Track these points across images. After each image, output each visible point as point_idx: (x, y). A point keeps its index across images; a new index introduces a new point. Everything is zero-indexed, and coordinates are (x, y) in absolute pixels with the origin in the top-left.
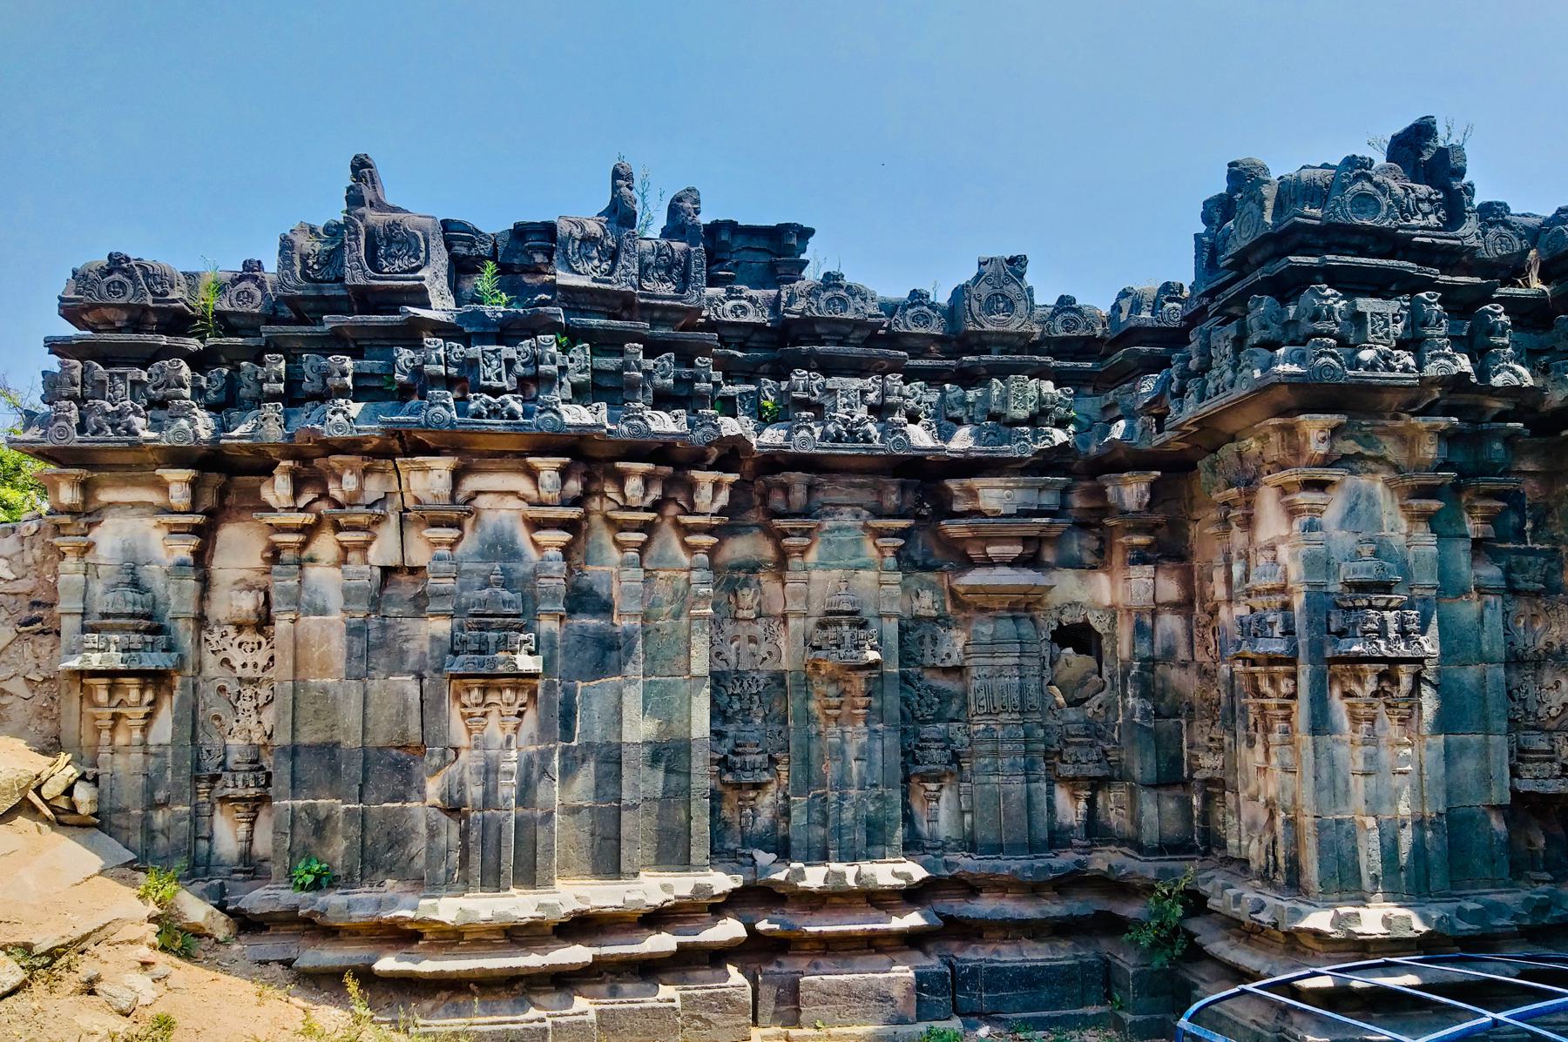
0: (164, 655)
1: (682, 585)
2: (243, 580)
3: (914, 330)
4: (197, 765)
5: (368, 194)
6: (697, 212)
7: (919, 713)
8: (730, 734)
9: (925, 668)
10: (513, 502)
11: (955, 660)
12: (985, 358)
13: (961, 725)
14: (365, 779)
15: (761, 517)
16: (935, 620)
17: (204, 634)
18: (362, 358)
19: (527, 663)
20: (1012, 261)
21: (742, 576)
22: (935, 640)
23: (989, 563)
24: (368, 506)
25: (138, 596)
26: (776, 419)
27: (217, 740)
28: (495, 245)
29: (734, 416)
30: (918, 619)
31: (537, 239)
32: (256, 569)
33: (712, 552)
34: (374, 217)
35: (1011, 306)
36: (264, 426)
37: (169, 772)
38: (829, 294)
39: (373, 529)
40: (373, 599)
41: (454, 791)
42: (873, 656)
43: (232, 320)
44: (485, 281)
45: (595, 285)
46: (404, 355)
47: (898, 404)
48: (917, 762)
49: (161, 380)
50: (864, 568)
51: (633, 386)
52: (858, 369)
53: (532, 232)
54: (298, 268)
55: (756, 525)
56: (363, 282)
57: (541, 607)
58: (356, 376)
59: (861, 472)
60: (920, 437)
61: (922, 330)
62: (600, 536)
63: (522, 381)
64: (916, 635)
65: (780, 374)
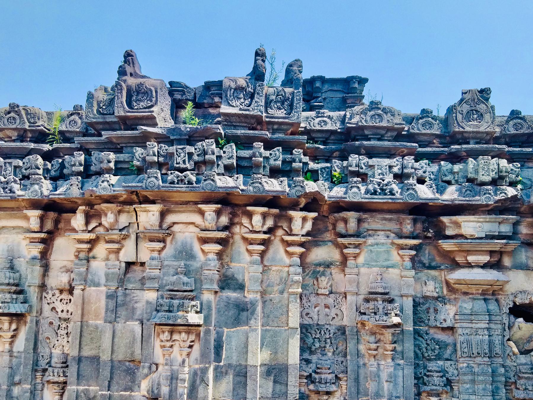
0: (21, 305)
1: (285, 275)
2: (65, 266)
3: (424, 132)
4: (36, 363)
5: (129, 69)
6: (301, 72)
7: (426, 355)
8: (314, 361)
9: (430, 327)
10: (192, 228)
11: (448, 324)
12: (464, 146)
13: (452, 363)
14: (111, 378)
15: (333, 237)
16: (436, 299)
17: (44, 294)
18: (121, 152)
19: (194, 318)
20: (482, 91)
21: (321, 269)
22: (436, 311)
23: (469, 265)
24: (120, 230)
25: (12, 274)
26: (342, 181)
27: (47, 350)
28: (195, 94)
29: (315, 181)
30: (426, 298)
31: (214, 89)
32: (72, 261)
33: (302, 256)
34: (132, 81)
35: (481, 116)
36: (70, 189)
37: (22, 366)
38: (372, 113)
39: (123, 242)
40: (121, 279)
41: (155, 389)
42: (396, 320)
43: (68, 135)
44: (186, 113)
45: (241, 112)
46: (139, 151)
47: (412, 173)
48: (425, 384)
49: (29, 165)
50: (392, 267)
51: (258, 166)
52: (389, 154)
53: (214, 86)
54: (95, 109)
55: (330, 241)
56: (123, 114)
57: (204, 287)
58: (116, 163)
59: (390, 211)
60: (425, 192)
61: (429, 132)
62: (239, 247)
63: (196, 163)
64: (425, 307)
65: (344, 157)
